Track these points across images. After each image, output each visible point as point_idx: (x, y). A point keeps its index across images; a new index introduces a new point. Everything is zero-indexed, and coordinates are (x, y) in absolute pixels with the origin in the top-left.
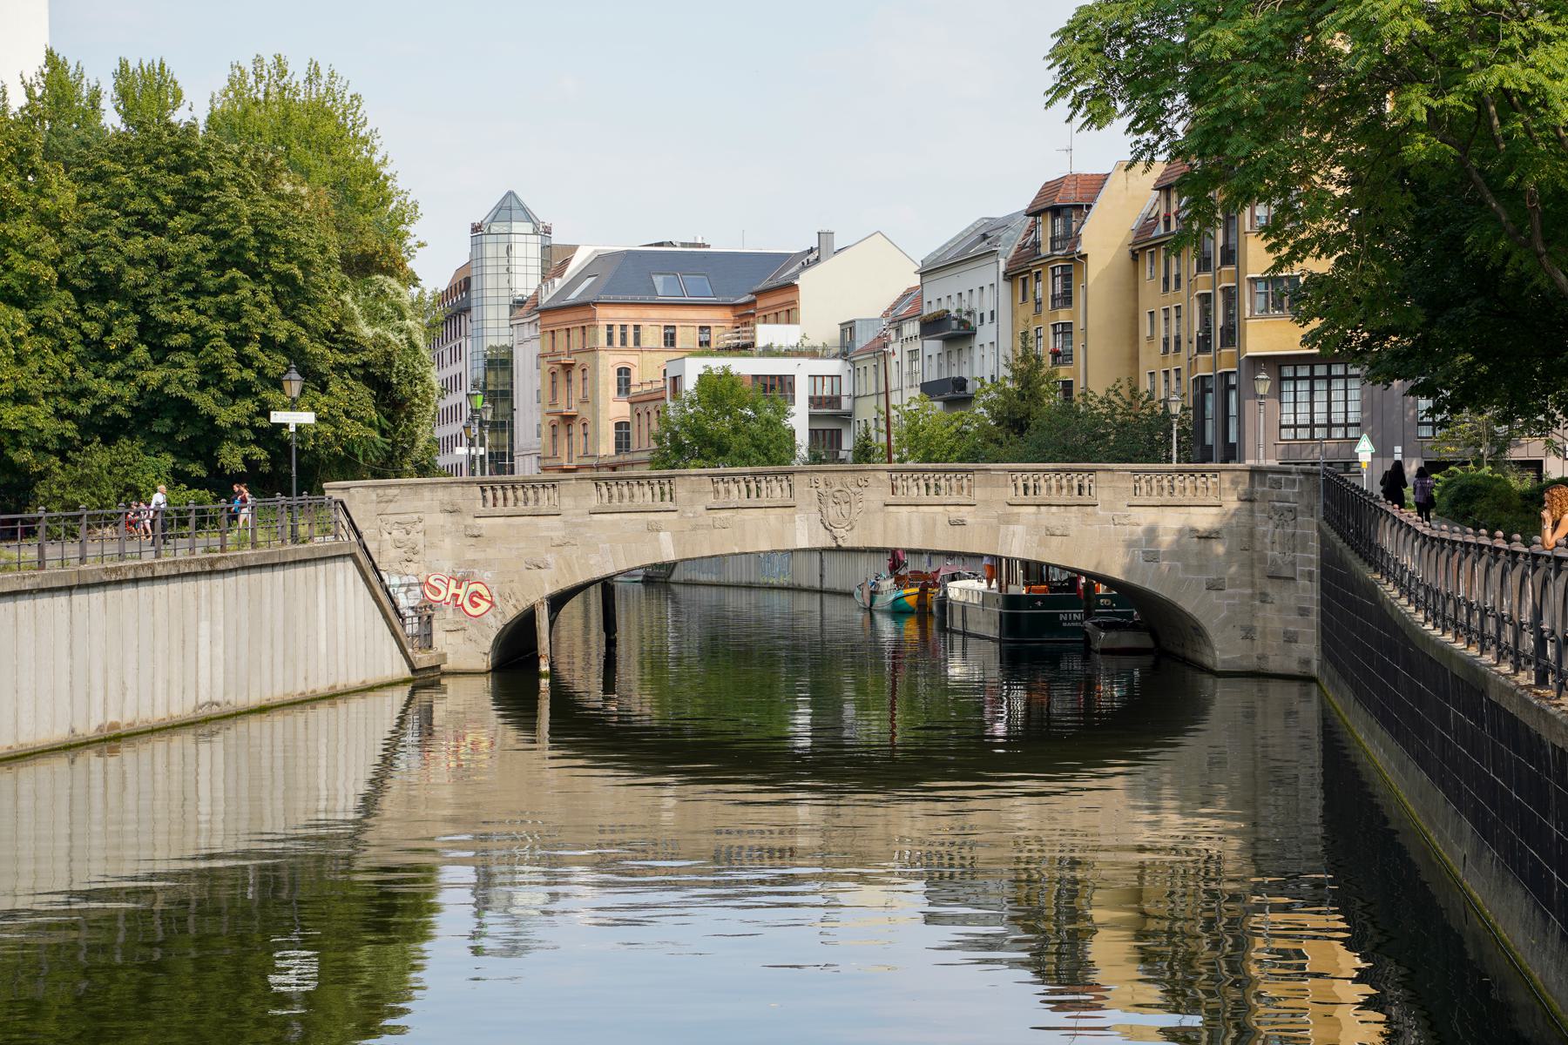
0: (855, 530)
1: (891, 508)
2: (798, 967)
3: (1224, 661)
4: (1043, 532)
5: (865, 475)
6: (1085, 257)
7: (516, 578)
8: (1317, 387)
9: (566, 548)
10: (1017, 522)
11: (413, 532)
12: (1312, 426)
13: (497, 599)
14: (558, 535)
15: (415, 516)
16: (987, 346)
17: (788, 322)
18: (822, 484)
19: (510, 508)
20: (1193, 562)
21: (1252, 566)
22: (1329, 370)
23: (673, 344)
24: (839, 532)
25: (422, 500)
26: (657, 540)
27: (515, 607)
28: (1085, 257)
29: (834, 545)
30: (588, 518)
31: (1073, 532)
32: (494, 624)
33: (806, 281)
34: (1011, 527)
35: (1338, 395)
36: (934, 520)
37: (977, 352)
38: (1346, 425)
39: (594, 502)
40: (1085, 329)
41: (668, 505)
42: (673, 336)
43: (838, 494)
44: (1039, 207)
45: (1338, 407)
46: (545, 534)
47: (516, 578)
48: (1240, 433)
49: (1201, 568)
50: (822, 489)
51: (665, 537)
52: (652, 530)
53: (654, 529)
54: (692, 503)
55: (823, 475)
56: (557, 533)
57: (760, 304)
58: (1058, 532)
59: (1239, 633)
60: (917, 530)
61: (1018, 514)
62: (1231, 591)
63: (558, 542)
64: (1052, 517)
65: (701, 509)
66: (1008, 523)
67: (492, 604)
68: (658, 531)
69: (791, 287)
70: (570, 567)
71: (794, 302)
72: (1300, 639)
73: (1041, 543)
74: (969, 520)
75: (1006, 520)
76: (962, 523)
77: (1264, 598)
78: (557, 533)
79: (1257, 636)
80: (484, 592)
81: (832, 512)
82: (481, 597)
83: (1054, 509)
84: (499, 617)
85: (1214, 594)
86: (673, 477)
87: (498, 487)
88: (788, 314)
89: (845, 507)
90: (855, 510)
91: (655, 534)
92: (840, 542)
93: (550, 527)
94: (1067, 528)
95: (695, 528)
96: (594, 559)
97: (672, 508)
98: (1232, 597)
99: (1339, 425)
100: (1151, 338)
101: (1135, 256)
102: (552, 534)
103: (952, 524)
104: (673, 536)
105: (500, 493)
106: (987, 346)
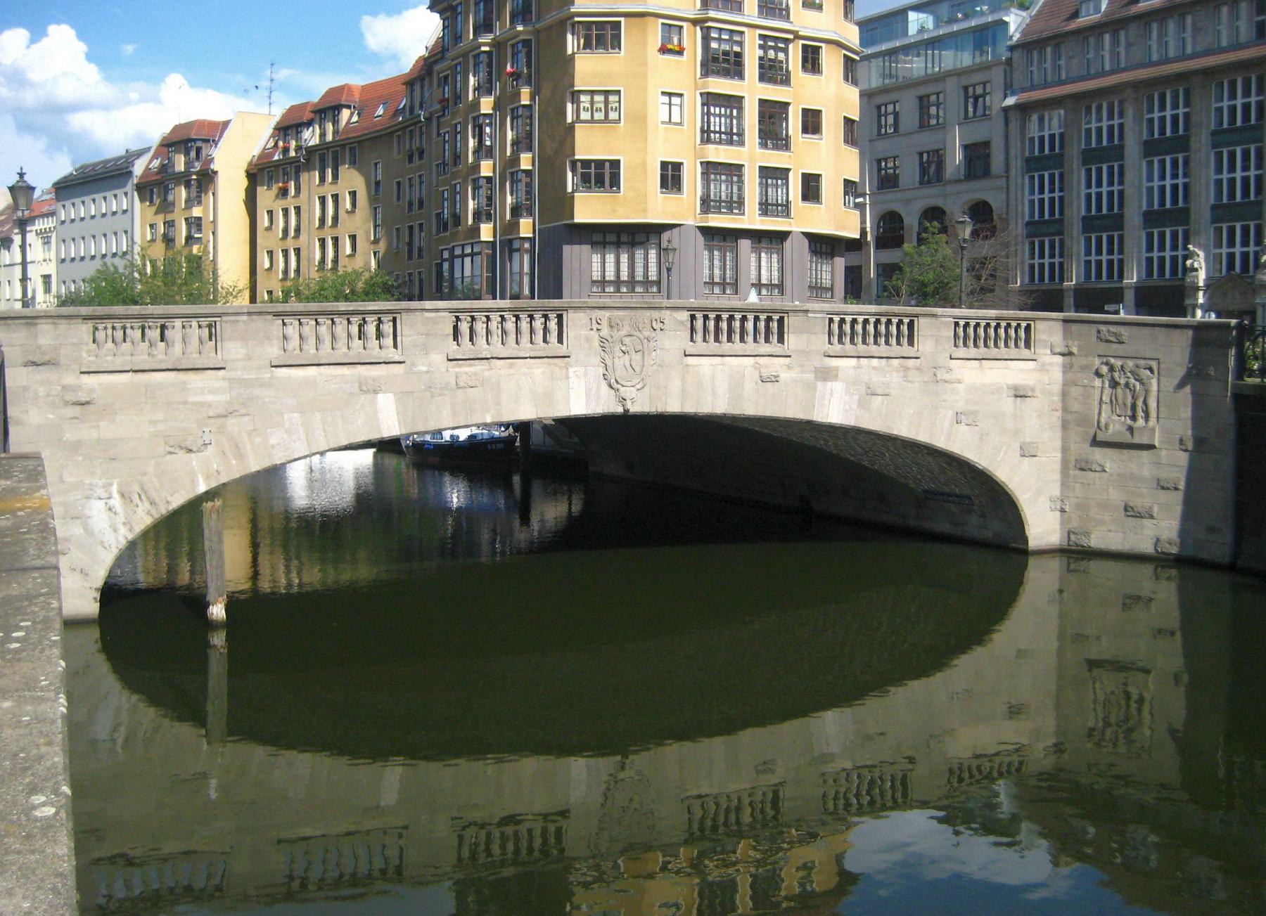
0: (647, 388)
1: (690, 360)
4: (863, 390)
6: (216, 173)
18: (605, 324)
22: (605, 238)
24: (628, 392)
26: (374, 403)
27: (149, 513)
28: (216, 173)
30: (267, 374)
34: (829, 384)
39: (273, 351)
40: (214, 222)
43: (627, 340)
50: (605, 332)
54: (426, 350)
55: (607, 314)
58: (879, 391)
60: (722, 387)
61: (837, 369)
65: (438, 359)
68: (376, 392)
73: (862, 404)
74: (784, 376)
76: (774, 380)
81: (621, 362)
86: (398, 312)
87: (523, 316)
89: (637, 358)
90: (649, 362)
91: (369, 396)
97: (397, 358)
100: (269, 229)
105: (524, 325)
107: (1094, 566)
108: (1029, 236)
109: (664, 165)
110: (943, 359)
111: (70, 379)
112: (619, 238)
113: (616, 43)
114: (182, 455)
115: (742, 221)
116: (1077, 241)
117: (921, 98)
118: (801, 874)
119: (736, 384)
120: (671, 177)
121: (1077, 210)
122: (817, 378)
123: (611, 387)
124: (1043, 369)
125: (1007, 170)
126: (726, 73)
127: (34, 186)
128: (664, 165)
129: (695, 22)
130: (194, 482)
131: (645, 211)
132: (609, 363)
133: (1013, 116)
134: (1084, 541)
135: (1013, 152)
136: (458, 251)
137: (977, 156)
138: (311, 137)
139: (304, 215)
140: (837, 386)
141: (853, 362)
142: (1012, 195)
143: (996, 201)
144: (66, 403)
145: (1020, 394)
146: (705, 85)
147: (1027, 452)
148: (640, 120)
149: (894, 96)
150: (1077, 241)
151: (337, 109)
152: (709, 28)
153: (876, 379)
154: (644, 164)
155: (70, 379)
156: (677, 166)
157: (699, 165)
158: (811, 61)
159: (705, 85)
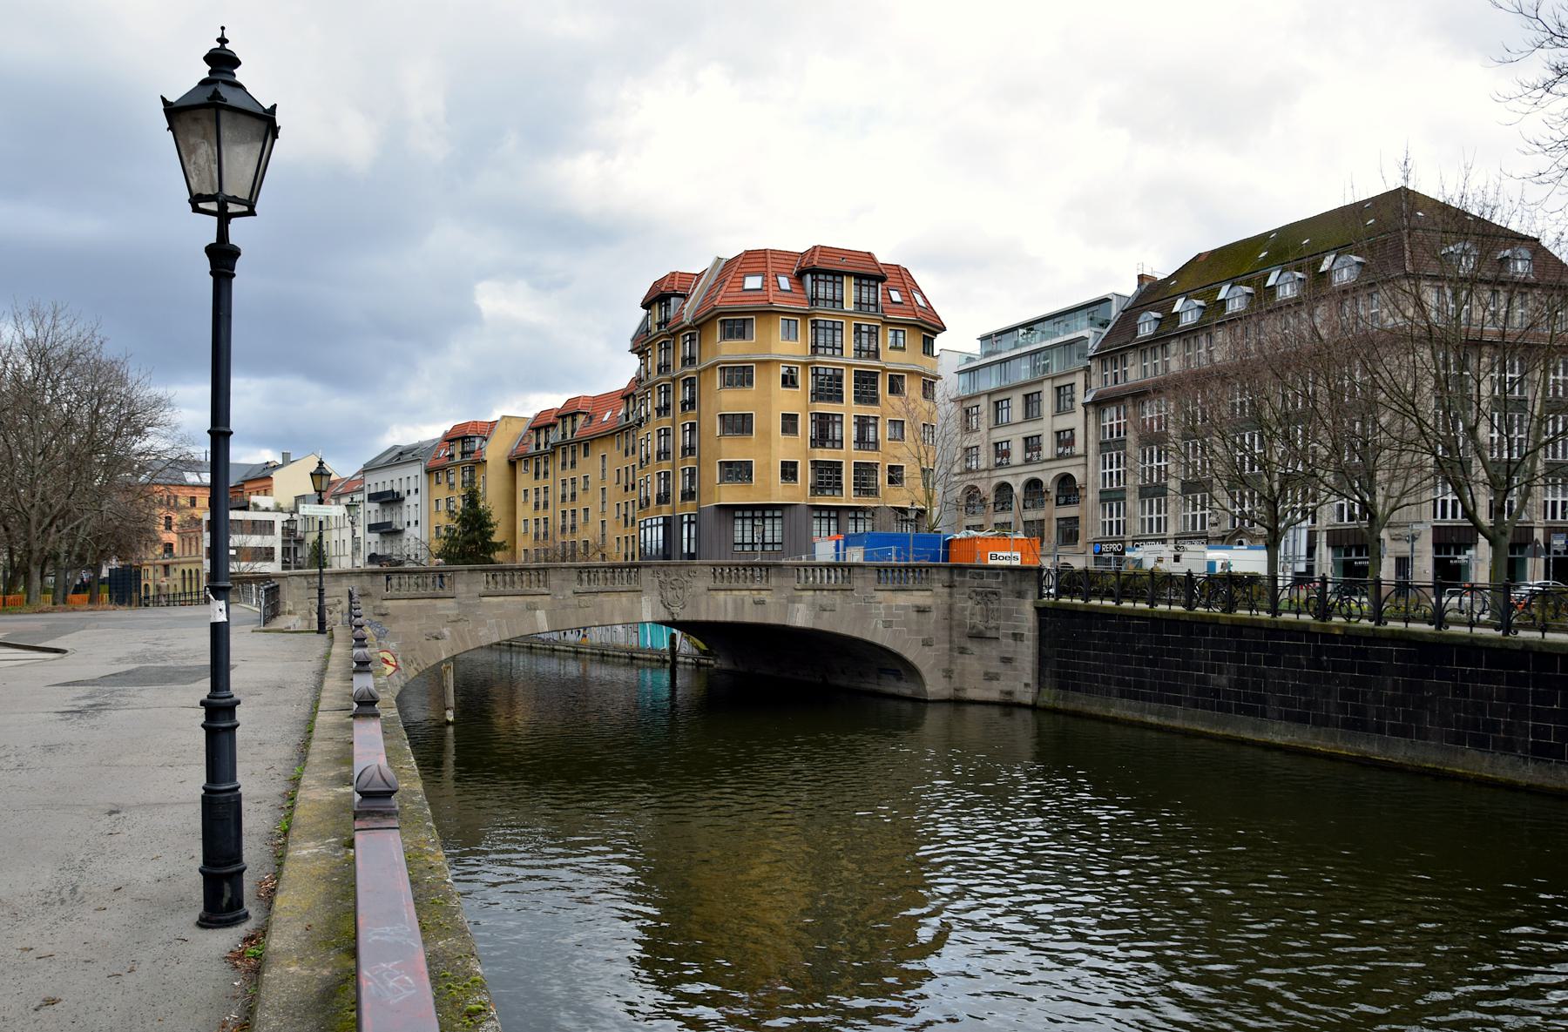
1: (712, 592)
2: (1012, 994)
3: (932, 693)
5: (693, 568)
7: (417, 647)
8: (756, 523)
9: (460, 623)
10: (800, 602)
11: (335, 612)
12: (753, 544)
13: (400, 664)
14: (453, 613)
15: (336, 599)
16: (412, 507)
17: (266, 495)
19: (518, 588)
20: (914, 627)
21: (951, 628)
23: (195, 505)
24: (676, 610)
25: (341, 586)
26: (534, 616)
27: (416, 669)
29: (671, 619)
31: (838, 608)
32: (398, 683)
33: (276, 475)
35: (768, 527)
36: (743, 600)
37: (405, 509)
38: (773, 544)
39: (482, 588)
41: (544, 590)
42: (195, 501)
44: (454, 436)
45: (768, 534)
46: (442, 612)
47: (417, 647)
48: (671, 551)
49: (919, 632)
51: (541, 615)
52: (531, 609)
53: (532, 608)
56: (452, 612)
57: (246, 487)
59: (940, 674)
60: (730, 606)
62: (937, 646)
63: (453, 619)
64: (825, 598)
65: (569, 593)
66: (794, 602)
67: (397, 668)
68: (535, 609)
69: (269, 478)
70: (462, 638)
71: (270, 486)
72: (1002, 678)
73: (817, 617)
74: (768, 600)
75: (792, 600)
76: (762, 602)
77: (963, 651)
78: (452, 612)
79: (955, 675)
80: (391, 659)
81: (670, 595)
82: (387, 662)
83: (825, 593)
84: (403, 678)
85: (927, 648)
88: (266, 492)
89: (680, 592)
90: (687, 594)
92: (676, 616)
93: (446, 607)
94: (834, 605)
95: (564, 607)
96: (483, 632)
97: (547, 592)
98: (937, 650)
99: (748, 544)
101: (512, 464)
102: (448, 612)
103: (756, 603)
104: (547, 614)
106: (412, 507)
107: (971, 709)
108: (1101, 501)
109: (784, 464)
110: (870, 589)
111: (377, 603)
112: (763, 513)
113: (750, 383)
114: (434, 641)
115: (841, 501)
116: (1132, 502)
117: (1026, 396)
118: (807, 901)
119: (739, 605)
120: (789, 471)
121: (1133, 482)
122: (788, 602)
123: (665, 607)
124: (936, 595)
125: (1086, 451)
126: (830, 399)
127: (256, 210)
128: (784, 464)
129: (806, 365)
130: (440, 655)
131: (770, 495)
132: (664, 594)
133: (1091, 410)
134: (962, 694)
135: (1090, 437)
136: (649, 523)
137: (1064, 439)
138: (555, 436)
139: (550, 494)
140: (801, 607)
141: (811, 593)
142: (1090, 470)
143: (1078, 475)
144: (375, 614)
145: (921, 610)
146: (814, 408)
147: (927, 643)
148: (766, 435)
149: (1007, 395)
150: (1132, 502)
151: (574, 415)
152: (817, 368)
153: (825, 602)
154: (769, 464)
155: (377, 603)
156: (795, 464)
157: (809, 463)
158: (895, 388)
159: (814, 408)
